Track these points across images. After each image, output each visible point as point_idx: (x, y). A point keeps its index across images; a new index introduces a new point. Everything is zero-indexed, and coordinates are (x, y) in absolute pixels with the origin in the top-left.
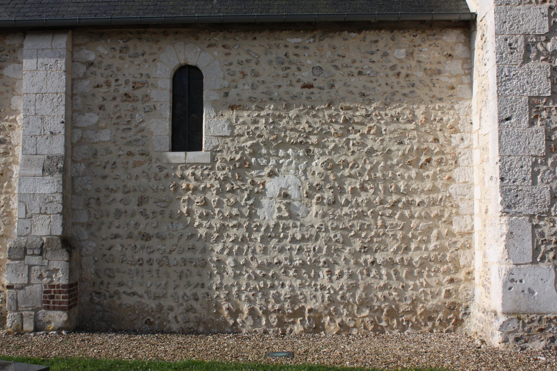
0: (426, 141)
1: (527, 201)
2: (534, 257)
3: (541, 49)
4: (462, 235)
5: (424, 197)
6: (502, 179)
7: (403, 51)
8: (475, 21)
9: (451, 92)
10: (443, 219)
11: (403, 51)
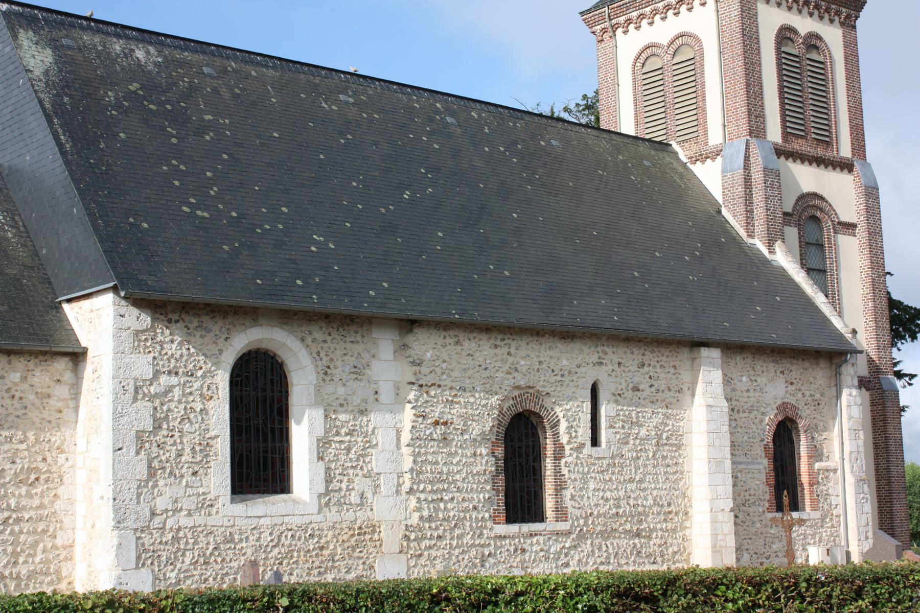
0: (36, 461)
1: (133, 517)
2: (137, 564)
3: (146, 391)
4: (65, 548)
5: (32, 513)
6: (114, 499)
7: (18, 375)
8: (86, 353)
9: (59, 415)
10: (49, 534)
11: (18, 375)
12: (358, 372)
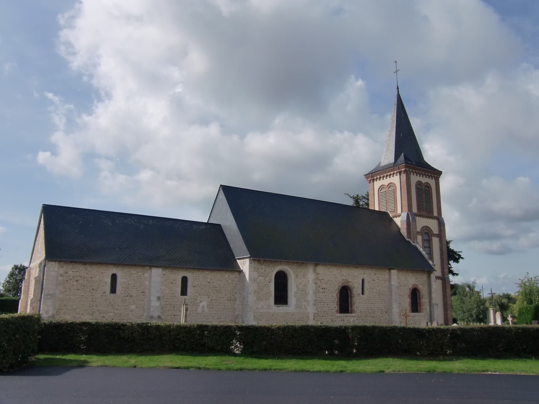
12: (304, 276)
